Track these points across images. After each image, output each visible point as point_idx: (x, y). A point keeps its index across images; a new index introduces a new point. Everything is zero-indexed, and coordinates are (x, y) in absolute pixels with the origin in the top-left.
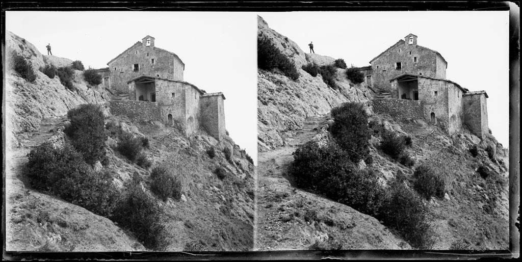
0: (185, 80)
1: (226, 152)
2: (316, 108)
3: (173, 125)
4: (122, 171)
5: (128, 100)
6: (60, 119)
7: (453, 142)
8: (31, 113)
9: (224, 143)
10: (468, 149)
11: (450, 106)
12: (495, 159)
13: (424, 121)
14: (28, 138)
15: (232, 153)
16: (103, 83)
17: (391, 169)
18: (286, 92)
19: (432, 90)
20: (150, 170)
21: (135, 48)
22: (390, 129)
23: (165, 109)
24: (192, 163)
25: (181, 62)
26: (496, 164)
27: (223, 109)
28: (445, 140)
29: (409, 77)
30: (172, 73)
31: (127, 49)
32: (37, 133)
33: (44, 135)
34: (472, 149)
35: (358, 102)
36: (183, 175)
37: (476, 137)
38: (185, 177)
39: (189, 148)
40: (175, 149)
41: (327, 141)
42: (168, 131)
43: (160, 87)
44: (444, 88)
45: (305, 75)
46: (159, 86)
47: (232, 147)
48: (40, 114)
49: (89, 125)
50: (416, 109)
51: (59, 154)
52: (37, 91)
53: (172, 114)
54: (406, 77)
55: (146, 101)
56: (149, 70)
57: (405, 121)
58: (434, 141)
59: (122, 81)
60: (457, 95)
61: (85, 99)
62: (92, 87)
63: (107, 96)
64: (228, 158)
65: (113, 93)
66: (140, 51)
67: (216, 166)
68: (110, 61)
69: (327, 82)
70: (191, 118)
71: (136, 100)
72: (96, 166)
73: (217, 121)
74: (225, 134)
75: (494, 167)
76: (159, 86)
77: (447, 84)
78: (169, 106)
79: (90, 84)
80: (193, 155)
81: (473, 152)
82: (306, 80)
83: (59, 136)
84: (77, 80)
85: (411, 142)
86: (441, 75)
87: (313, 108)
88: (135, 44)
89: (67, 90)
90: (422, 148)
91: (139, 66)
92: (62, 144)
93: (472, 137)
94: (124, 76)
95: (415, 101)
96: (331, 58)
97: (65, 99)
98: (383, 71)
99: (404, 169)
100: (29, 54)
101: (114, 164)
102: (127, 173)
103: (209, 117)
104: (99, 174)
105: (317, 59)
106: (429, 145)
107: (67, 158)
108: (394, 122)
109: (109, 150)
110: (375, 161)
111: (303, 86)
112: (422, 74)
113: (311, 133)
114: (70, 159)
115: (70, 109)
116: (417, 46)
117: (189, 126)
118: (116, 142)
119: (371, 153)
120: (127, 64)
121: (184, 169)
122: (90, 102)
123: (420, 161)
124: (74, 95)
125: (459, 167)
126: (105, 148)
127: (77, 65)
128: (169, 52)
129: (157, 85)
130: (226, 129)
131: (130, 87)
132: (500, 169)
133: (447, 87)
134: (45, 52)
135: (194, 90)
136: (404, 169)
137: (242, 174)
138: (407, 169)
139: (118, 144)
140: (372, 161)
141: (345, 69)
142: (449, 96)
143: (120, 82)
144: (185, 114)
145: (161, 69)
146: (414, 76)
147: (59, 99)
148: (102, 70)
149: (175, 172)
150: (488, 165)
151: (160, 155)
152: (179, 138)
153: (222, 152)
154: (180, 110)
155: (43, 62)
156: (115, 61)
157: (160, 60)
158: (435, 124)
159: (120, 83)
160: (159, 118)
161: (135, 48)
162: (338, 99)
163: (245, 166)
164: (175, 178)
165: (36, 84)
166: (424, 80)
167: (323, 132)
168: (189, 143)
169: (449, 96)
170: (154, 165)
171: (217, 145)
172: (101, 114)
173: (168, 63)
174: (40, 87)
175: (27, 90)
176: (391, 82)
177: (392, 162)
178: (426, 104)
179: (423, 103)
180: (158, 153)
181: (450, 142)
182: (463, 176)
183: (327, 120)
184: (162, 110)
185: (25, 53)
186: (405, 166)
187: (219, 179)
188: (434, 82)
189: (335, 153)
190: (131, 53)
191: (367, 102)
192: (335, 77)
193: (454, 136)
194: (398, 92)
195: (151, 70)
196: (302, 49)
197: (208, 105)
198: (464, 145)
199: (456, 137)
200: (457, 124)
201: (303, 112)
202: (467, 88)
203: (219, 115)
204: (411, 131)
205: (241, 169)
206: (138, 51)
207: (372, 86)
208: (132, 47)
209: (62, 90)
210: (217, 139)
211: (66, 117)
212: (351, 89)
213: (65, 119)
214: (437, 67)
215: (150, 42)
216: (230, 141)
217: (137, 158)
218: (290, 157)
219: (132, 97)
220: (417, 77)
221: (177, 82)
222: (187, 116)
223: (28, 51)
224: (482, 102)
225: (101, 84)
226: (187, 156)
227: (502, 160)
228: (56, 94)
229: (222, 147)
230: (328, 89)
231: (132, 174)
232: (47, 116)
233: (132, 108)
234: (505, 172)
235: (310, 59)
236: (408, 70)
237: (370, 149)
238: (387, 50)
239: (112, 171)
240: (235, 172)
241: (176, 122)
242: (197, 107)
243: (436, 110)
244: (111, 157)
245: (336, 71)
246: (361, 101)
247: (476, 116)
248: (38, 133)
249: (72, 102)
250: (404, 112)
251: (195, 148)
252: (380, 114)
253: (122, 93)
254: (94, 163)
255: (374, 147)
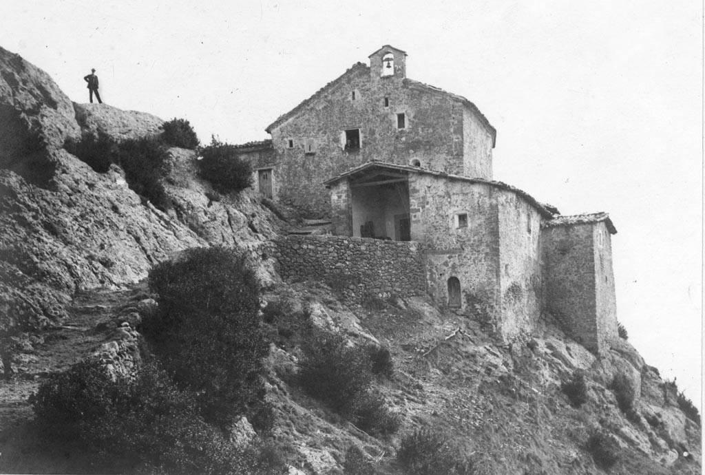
0: (497, 178)
1: (620, 387)
2: (107, 264)
3: (463, 308)
4: (312, 445)
5: (330, 235)
6: (126, 293)
7: (515, 362)
8: (42, 276)
9: (613, 362)
10: (558, 383)
11: (504, 258)
12: (639, 413)
13: (427, 301)
14: (31, 347)
15: (638, 390)
16: (256, 185)
17: (327, 442)
18: (15, 218)
19: (450, 212)
20: (396, 441)
21: (349, 82)
22: (328, 325)
23: (438, 261)
24: (520, 420)
25: (483, 122)
26: (641, 428)
27: (611, 263)
28: (490, 358)
29: (386, 174)
30: (460, 155)
31: (323, 86)
32: (59, 333)
33: (80, 339)
34: (569, 385)
35: (232, 245)
36: (494, 456)
37: (582, 347)
38: (500, 462)
39: (509, 376)
40: (468, 379)
41: (134, 362)
42: (448, 327)
43: (424, 198)
44: (487, 206)
45: (75, 167)
46: (422, 193)
47: (637, 374)
48: (67, 277)
49: (216, 311)
50: (404, 266)
51: (126, 397)
52: (58, 211)
53: (459, 277)
54: (375, 172)
55: (382, 238)
56: (392, 148)
57: (371, 303)
58: (459, 360)
59: (309, 178)
60: (524, 226)
61: (200, 235)
62: (221, 196)
63: (266, 225)
64: (625, 405)
65: (285, 214)
66: (364, 92)
67: (591, 430)
68: (275, 119)
69: (141, 187)
70: (515, 289)
71: (352, 235)
72: (235, 431)
73: (593, 297)
74: (617, 334)
75: (633, 437)
76: (422, 193)
77: (496, 193)
78: (451, 252)
79: (214, 188)
80: (522, 398)
81: (573, 391)
82: (77, 182)
83: (125, 343)
84: (177, 179)
85: (390, 365)
86: (478, 167)
87: (98, 265)
88: (349, 71)
89: (147, 207)
90: (421, 382)
91: (361, 136)
92: (132, 365)
93: (568, 349)
94: (318, 166)
95: (400, 244)
96: (152, 117)
97: (141, 234)
98: (308, 154)
99: (367, 444)
100: (34, 101)
101: (288, 425)
102: (326, 452)
103: (568, 285)
104: (245, 454)
105: (110, 121)
106: (444, 372)
107: (150, 408)
108: (339, 306)
109: (272, 383)
110: (281, 420)
111: (66, 201)
112: (423, 164)
113: (90, 338)
114: (158, 411)
115: (156, 263)
116: (406, 83)
117: (510, 313)
118: (296, 359)
119: (269, 398)
120: (324, 130)
121: (495, 438)
122: (217, 241)
123: (416, 419)
124: (167, 223)
125: (533, 437)
126: (263, 380)
127: (179, 133)
128: (450, 96)
129: (416, 191)
130: (619, 320)
131: (334, 197)
132: (652, 441)
133: (494, 202)
134: (79, 94)
135: (523, 206)
136: (367, 444)
137: (665, 451)
138: (376, 443)
139: (299, 364)
140: (273, 419)
141: (190, 148)
142: (501, 229)
143: (305, 182)
144: (498, 276)
145: (427, 146)
146: (397, 171)
147: (123, 234)
148: (250, 148)
149: (470, 448)
150: (617, 431)
151: (424, 396)
152: (481, 349)
153: (608, 388)
154: (484, 266)
155: (75, 124)
156: (291, 120)
157: (421, 117)
158: (460, 312)
159: (305, 187)
160: (421, 289)
161: (349, 82)
162: (171, 238)
163: (676, 430)
164: (471, 465)
165: (54, 187)
166: (427, 181)
167: (124, 336)
168: (510, 362)
169: (502, 229)
170: (407, 427)
171: (594, 366)
172: (248, 277)
173: (448, 125)
174: (66, 197)
175: (28, 206)
176: (329, 188)
177: (333, 421)
178: (434, 252)
179: (428, 248)
180: (417, 391)
181: (506, 364)
182: (545, 464)
183: (138, 299)
184: (431, 264)
185: (21, 96)
186: (372, 434)
187: (599, 466)
188: (457, 187)
189: (155, 399)
190: (337, 97)
191: (260, 247)
192: (164, 174)
193: (516, 347)
194: (350, 218)
195: (395, 148)
196: (66, 92)
197: (564, 251)
198: (546, 372)
199: (522, 348)
200: (526, 310)
201: (67, 277)
202: (553, 204)
203: (597, 281)
204: (389, 332)
205: (665, 436)
206: (356, 91)
207: (276, 200)
208: (340, 79)
209: (134, 206)
210: (593, 349)
211: (144, 286)
212: (211, 209)
213: (142, 293)
214: (466, 145)
215: (392, 63)
216: (631, 356)
217: (357, 405)
218: (22, 409)
219: (341, 228)
220: (407, 173)
221: (473, 182)
222: (505, 284)
223: (31, 92)
224: (598, 246)
225: (248, 189)
226: (504, 400)
227: (659, 415)
228: (114, 217)
229: (608, 372)
230: (141, 207)
231: (343, 453)
232: (90, 284)
233: (341, 259)
234: (665, 451)
235: (89, 119)
236: (379, 153)
237: (268, 385)
238: (319, 93)
239: (282, 444)
240: (646, 447)
241: (471, 299)
242: (534, 256)
243: (463, 269)
244: (280, 405)
245: (167, 156)
246: (242, 244)
247: (580, 287)
248: (62, 333)
249: (162, 243)
250: (368, 276)
251: (528, 378)
252: (298, 281)
253: (310, 215)
254: (231, 422)
255: (278, 380)
